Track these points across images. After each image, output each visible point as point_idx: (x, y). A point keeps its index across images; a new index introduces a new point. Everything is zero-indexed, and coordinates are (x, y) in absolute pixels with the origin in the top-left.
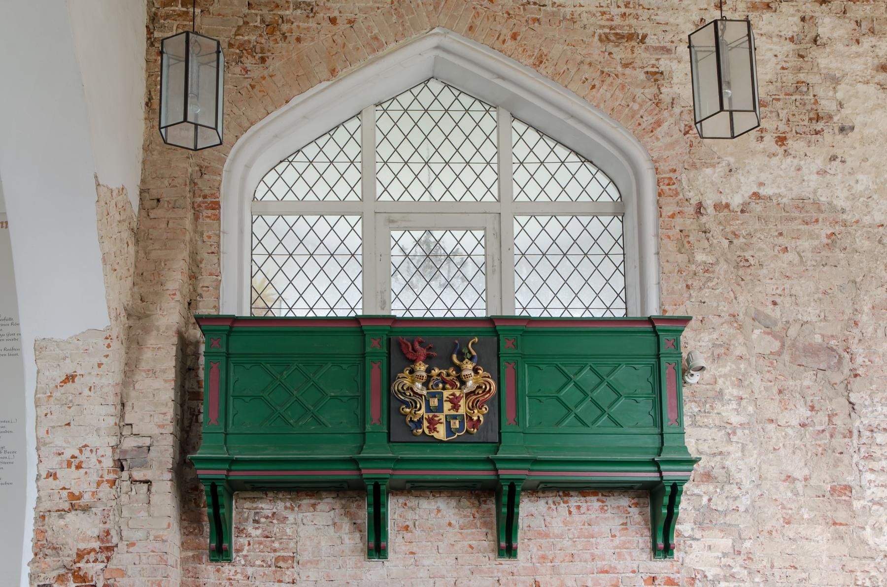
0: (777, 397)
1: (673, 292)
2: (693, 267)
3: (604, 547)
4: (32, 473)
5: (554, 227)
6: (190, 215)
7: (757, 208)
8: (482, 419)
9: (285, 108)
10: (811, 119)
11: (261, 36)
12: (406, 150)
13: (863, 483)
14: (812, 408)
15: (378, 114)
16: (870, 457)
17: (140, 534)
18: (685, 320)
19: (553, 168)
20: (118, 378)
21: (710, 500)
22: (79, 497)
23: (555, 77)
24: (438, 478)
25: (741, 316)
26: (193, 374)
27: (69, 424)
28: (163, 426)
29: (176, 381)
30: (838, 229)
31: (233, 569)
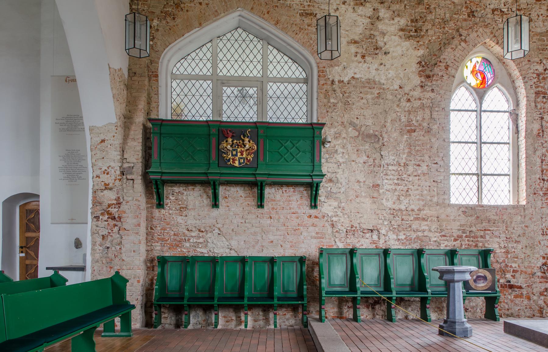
0: (356, 153)
1: (322, 113)
2: (330, 104)
3: (294, 205)
4: (91, 176)
5: (282, 87)
6: (147, 80)
7: (353, 82)
8: (251, 159)
9: (182, 38)
10: (374, 49)
11: (173, 9)
12: (229, 56)
13: (384, 184)
14: (368, 157)
15: (218, 41)
16: (386, 174)
17: (130, 198)
18: (323, 124)
19: (282, 64)
20: (121, 141)
21: (331, 189)
22: (108, 185)
23: (284, 29)
24: (236, 180)
25: (345, 123)
26: (149, 140)
27: (103, 158)
28: (138, 159)
29: (142, 143)
30: (381, 91)
31: (165, 211)
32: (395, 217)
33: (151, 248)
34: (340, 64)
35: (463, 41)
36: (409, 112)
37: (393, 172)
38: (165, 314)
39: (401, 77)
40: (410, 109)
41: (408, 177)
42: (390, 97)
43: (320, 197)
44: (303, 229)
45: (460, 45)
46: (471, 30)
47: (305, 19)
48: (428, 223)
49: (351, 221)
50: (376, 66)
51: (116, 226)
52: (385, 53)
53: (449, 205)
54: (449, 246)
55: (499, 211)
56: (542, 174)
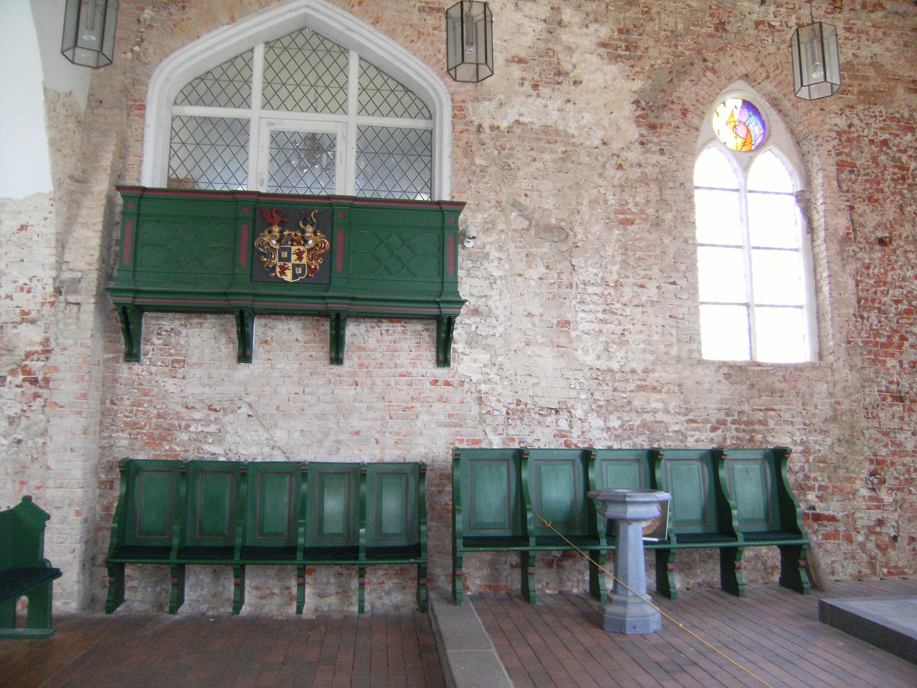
0: (525, 259)
2: (474, 168)
3: (404, 358)
10: (555, 74)
13: (578, 319)
14: (548, 267)
16: (582, 302)
21: (477, 328)
30: (570, 148)
31: (141, 367)
32: (601, 385)
33: (109, 443)
34: (492, 97)
35: (709, 70)
36: (622, 187)
37: (595, 298)
38: (133, 580)
39: (605, 124)
40: (623, 183)
41: (624, 307)
42: (585, 159)
43: (455, 343)
44: (422, 406)
45: (705, 76)
46: (721, 53)
47: (428, 18)
48: (663, 396)
49: (516, 392)
50: (559, 103)
51: (40, 396)
52: (575, 83)
53: (701, 362)
54: (703, 441)
55: (788, 373)
56: (859, 307)
